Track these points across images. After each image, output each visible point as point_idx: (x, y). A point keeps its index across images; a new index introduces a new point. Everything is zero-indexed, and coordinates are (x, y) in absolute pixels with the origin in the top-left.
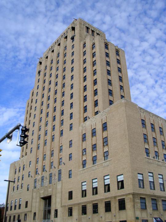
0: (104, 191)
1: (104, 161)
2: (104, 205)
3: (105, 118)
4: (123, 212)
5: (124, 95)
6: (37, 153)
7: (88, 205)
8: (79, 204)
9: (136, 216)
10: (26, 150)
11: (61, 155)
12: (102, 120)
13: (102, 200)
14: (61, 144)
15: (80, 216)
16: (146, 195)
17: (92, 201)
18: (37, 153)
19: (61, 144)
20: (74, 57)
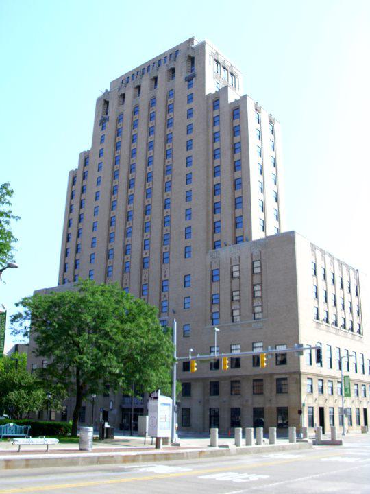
0: (252, 365)
1: (231, 324)
2: (250, 384)
3: (258, 253)
4: (281, 396)
5: (4, 308)
6: (123, 279)
7: (223, 382)
8: (204, 379)
9: (193, 383)
10: (213, 217)
11: (165, 296)
12: (252, 254)
13: (248, 377)
14: (165, 276)
15: (206, 398)
16: (313, 374)
17: (231, 377)
18: (123, 279)
19: (165, 276)
20: (192, 120)
